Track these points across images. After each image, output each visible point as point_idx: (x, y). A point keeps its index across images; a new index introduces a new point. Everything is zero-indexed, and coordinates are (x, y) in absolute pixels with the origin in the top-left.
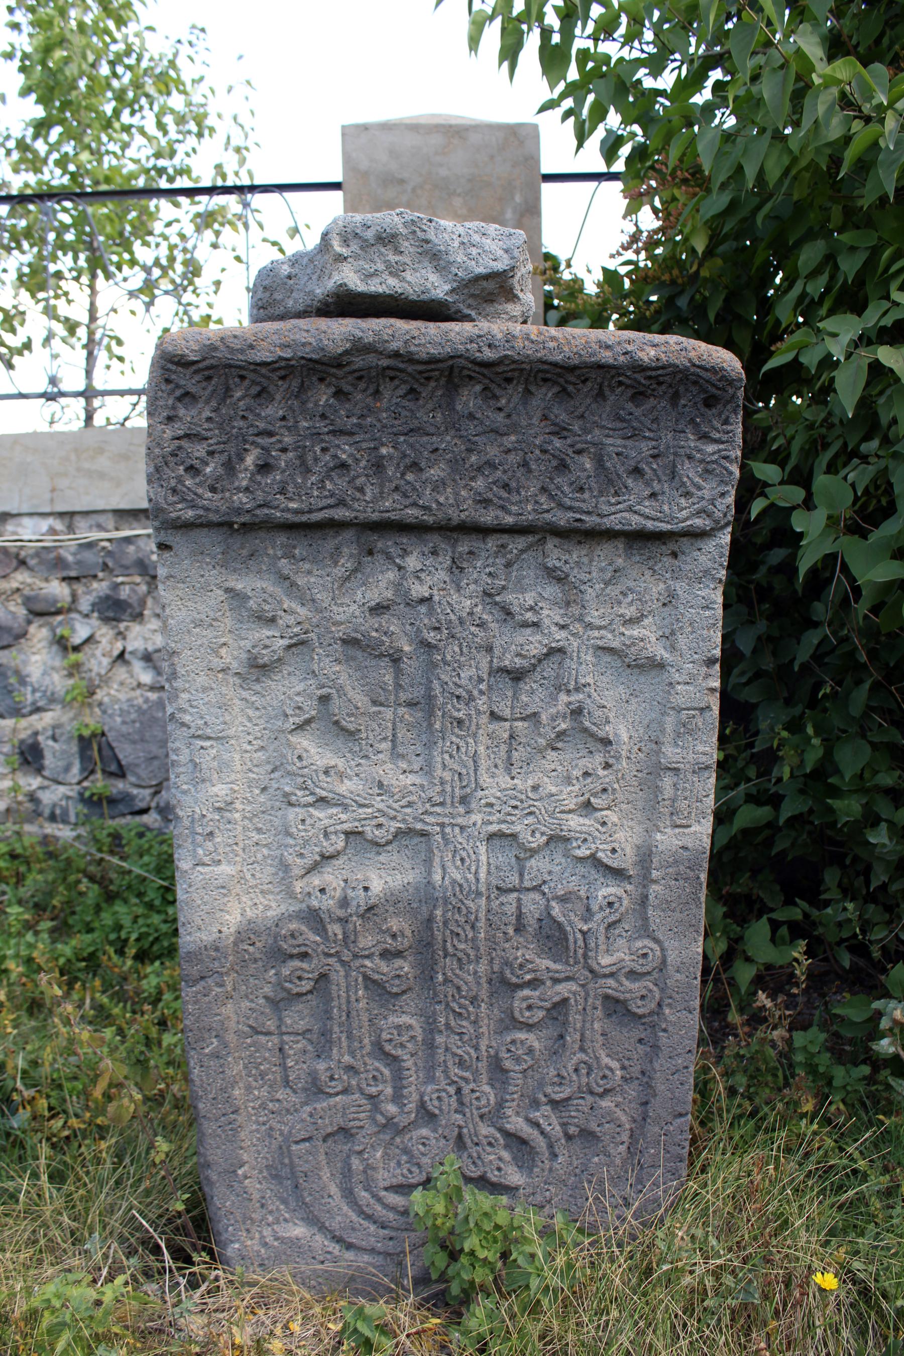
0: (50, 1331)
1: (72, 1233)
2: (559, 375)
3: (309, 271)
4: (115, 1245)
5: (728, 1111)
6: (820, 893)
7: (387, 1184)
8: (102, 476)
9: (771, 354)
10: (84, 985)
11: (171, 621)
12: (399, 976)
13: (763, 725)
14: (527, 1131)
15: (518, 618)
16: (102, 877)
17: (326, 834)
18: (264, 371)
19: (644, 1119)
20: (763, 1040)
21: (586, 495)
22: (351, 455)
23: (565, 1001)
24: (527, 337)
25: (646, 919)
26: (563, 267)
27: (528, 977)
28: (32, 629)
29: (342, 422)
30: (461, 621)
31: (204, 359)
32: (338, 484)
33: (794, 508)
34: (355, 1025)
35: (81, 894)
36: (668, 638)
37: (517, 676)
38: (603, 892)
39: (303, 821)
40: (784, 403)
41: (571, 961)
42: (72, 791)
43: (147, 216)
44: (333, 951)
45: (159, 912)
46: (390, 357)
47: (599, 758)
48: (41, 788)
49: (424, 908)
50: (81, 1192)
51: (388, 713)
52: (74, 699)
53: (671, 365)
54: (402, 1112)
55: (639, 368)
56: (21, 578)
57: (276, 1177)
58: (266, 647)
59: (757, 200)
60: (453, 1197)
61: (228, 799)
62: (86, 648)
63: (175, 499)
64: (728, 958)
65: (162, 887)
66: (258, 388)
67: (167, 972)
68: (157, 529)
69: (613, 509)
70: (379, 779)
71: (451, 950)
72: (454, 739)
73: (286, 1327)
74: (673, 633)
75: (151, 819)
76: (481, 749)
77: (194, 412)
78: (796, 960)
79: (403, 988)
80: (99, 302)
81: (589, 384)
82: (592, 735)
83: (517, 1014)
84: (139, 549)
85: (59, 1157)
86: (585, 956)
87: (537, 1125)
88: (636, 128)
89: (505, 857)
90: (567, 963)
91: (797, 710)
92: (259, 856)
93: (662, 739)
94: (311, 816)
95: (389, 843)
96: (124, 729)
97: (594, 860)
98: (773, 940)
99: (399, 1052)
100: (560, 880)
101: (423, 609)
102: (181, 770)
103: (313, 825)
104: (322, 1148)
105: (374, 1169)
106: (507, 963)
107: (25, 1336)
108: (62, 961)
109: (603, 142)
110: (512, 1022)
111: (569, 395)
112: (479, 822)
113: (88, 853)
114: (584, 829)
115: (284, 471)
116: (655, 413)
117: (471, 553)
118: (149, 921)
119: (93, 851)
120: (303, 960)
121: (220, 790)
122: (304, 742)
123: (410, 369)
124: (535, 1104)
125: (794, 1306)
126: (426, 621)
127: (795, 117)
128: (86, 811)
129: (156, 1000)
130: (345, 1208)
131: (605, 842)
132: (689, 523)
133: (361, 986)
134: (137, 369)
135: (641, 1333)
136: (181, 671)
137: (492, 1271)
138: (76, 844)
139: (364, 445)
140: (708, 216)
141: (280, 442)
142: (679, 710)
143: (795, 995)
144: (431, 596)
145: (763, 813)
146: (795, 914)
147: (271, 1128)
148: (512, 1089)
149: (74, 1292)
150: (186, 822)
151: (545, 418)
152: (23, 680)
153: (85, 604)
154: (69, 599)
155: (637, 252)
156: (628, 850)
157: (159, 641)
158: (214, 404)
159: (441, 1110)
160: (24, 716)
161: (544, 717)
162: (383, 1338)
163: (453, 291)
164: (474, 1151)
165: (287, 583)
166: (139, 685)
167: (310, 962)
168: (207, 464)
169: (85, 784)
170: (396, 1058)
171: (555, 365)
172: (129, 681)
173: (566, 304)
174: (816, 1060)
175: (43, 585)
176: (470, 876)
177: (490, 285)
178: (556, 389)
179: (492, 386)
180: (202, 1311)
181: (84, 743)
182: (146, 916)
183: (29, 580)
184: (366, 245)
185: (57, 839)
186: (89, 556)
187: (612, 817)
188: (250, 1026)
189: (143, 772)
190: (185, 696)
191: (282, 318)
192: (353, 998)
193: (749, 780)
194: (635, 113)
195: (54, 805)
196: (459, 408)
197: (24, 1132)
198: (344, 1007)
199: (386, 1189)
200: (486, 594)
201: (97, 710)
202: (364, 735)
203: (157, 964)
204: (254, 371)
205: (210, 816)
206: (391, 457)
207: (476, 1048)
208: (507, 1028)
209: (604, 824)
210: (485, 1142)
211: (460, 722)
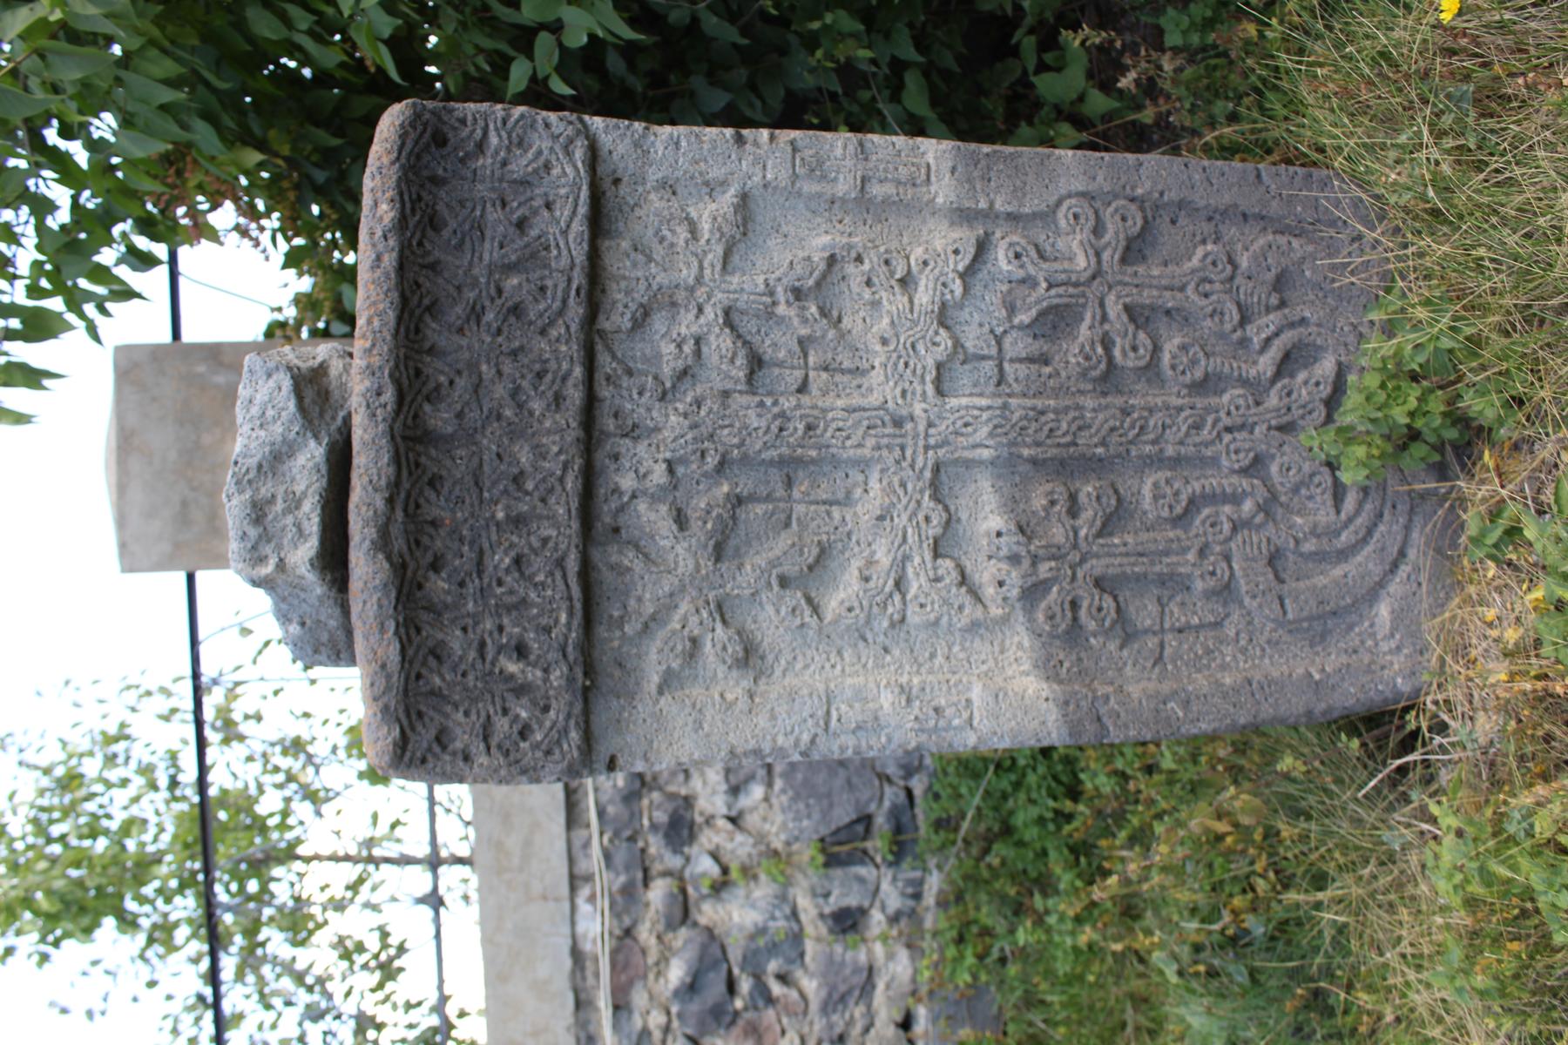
0: (1489, 885)
1: (1383, 864)
2: (412, 314)
3: (296, 602)
4: (1396, 816)
5: (1255, 122)
6: (1005, 16)
7: (1332, 511)
8: (528, 843)
9: (381, 70)
10: (1106, 859)
11: (696, 756)
12: (1098, 498)
13: (810, 81)
14: (1274, 352)
15: (690, 361)
16: (985, 839)
17: (937, 580)
18: (410, 652)
19: (1263, 218)
20: (1174, 82)
21: (549, 283)
22: (506, 553)
23: (1127, 308)
24: (368, 351)
25: (1035, 216)
26: (280, 317)
27: (1100, 350)
28: (703, 921)
29: (467, 560)
30: (694, 426)
31: (398, 720)
32: (539, 568)
33: (560, 45)
34: (1153, 547)
35: (1003, 863)
36: (712, 188)
37: (756, 363)
38: (1004, 265)
39: (922, 606)
40: (434, 56)
41: (1081, 301)
42: (887, 875)
43: (225, 797)
44: (1069, 572)
45: (1024, 775)
46: (393, 509)
47: (851, 269)
48: (883, 909)
49: (1021, 469)
50: (1337, 855)
51: (799, 509)
52: (782, 873)
53: (398, 185)
54: (1252, 494)
55: (402, 223)
56: (645, 934)
57: (1323, 636)
58: (724, 648)
59: (201, 89)
60: (1348, 436)
61: (897, 690)
62: (725, 859)
63: (557, 751)
64: (1080, 122)
65: (996, 772)
66: (431, 658)
67: (1093, 765)
68: (592, 772)
69: (564, 252)
70: (875, 522)
71: (1068, 439)
72: (829, 434)
73: (1490, 625)
74: (707, 184)
75: (918, 785)
76: (840, 403)
77: (458, 731)
78: (1083, 43)
79: (1111, 492)
80: (326, 852)
81: (421, 280)
82: (824, 276)
83: (1142, 363)
84: (611, 801)
85: (1298, 880)
86: (1076, 285)
87: (1268, 341)
88: (117, 230)
89: (963, 377)
90: (1084, 306)
91: (792, 38)
92: (962, 655)
93: (828, 196)
94: (916, 597)
95: (946, 509)
96: (816, 816)
97: (966, 275)
98: (1059, 70)
99: (1184, 497)
100: (989, 313)
101: (680, 470)
102: (864, 744)
103: (927, 595)
104: (1292, 584)
105: (1315, 526)
106: (1084, 374)
107: (1493, 912)
108: (1079, 883)
109: (135, 269)
110: (1151, 370)
111: (434, 303)
112: (924, 405)
113: (957, 856)
114: (931, 285)
115: (525, 629)
116: (454, 203)
117: (616, 416)
118: (1034, 786)
119: (954, 850)
120: (1078, 608)
121: (887, 700)
122: (832, 604)
123: (406, 485)
124: (1244, 342)
125: (1478, 45)
126: (694, 466)
127: (101, 42)
128: (909, 859)
129: (1124, 777)
130: (1359, 558)
131: (946, 261)
132: (580, 165)
133: (1108, 541)
134: (406, 796)
135: (1504, 221)
136: (752, 744)
137: (1431, 391)
138: (947, 868)
139: (494, 537)
140: (219, 144)
141: (491, 633)
142: (795, 176)
143: (1123, 45)
144: (666, 460)
145: (913, 81)
146: (1028, 44)
147: (1269, 642)
148: (1226, 369)
149: (1447, 858)
150: (923, 738)
151: (460, 331)
152: (761, 931)
153: (675, 862)
154: (668, 880)
155: (262, 229)
156: (956, 235)
157: (715, 776)
158: (449, 709)
159: (1250, 450)
160: (801, 929)
161: (804, 331)
162: (1506, 514)
163: (316, 437)
164: (1297, 413)
165: (652, 625)
166: (766, 799)
167: (1081, 598)
168: (517, 716)
169: (878, 859)
170: (1191, 501)
171: (399, 319)
172: (761, 811)
173: (329, 309)
174: (1198, 20)
175: (652, 908)
176: (985, 416)
177: (309, 394)
178: (427, 318)
179: (425, 391)
180: (1471, 718)
181: (832, 861)
182: (1029, 791)
183: (648, 925)
184: (266, 537)
185: (941, 892)
186: (620, 857)
187: (917, 254)
188: (1154, 665)
189: (865, 795)
190: (780, 740)
191: (349, 633)
192: (1122, 549)
193: (874, 99)
194: (100, 231)
195: (903, 894)
196: (450, 430)
197: (1269, 920)
198: (1132, 559)
199: (1338, 512)
200: (663, 398)
201: (795, 847)
202: (825, 537)
203: (1082, 776)
204: (411, 663)
205: (916, 711)
206: (507, 508)
207: (1180, 409)
208: (1158, 375)
209: (925, 263)
210: (1286, 400)
211: (809, 428)
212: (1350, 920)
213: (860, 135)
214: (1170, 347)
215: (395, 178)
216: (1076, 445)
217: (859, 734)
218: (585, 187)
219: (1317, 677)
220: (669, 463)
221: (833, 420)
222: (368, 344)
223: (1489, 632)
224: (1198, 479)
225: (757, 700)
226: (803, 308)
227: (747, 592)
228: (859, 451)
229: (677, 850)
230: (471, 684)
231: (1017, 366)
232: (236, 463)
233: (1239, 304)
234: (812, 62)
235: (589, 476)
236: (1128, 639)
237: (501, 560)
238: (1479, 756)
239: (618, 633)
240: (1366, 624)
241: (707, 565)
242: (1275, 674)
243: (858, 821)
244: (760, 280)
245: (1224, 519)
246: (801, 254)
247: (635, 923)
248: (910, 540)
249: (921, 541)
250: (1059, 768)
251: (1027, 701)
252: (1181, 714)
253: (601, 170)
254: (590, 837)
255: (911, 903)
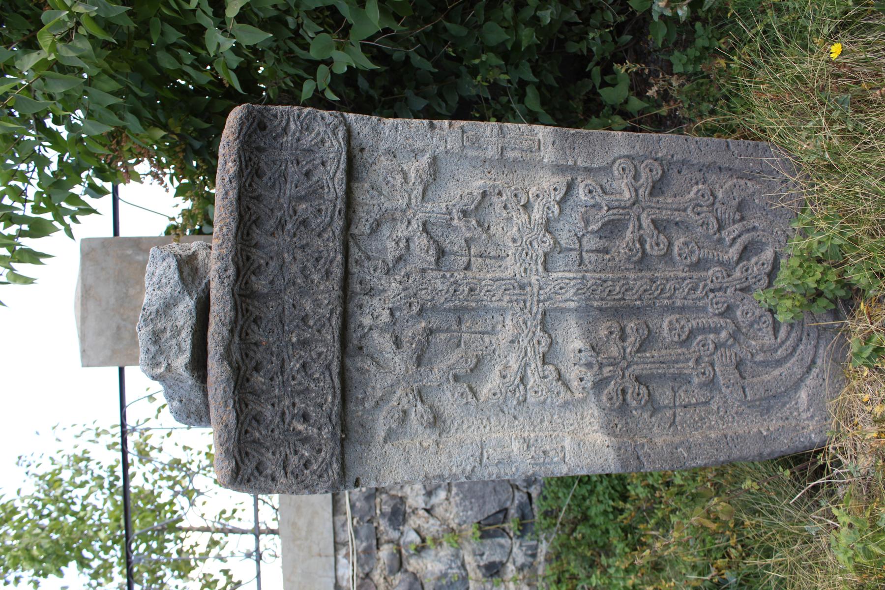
0: (869, 558)
1: (805, 543)
2: (245, 225)
3: (177, 389)
5: (725, 115)
7: (773, 337)
8: (310, 524)
9: (231, 87)
11: (405, 479)
15: (403, 252)
17: (545, 377)
18: (242, 418)
19: (730, 170)
20: (678, 91)
21: (323, 207)
22: (297, 361)
23: (653, 221)
27: (638, 245)
28: (411, 569)
29: (275, 361)
31: (235, 457)
32: (316, 370)
33: (332, 72)
34: (669, 358)
35: (583, 537)
36: (416, 154)
37: (441, 253)
38: (582, 197)
39: (536, 392)
40: (263, 78)
41: (627, 217)
42: (517, 543)
44: (621, 373)
45: (595, 487)
47: (495, 199)
48: (514, 563)
50: (778, 537)
51: (466, 336)
52: (456, 542)
53: (238, 152)
54: (726, 327)
57: (768, 410)
58: (422, 416)
59: (131, 96)
60: (781, 294)
61: (521, 441)
62: (423, 534)
63: (325, 476)
64: (625, 115)
65: (579, 484)
66: (253, 422)
67: (635, 481)
68: (345, 488)
69: (332, 190)
70: (508, 343)
71: (620, 296)
72: (482, 294)
73: (866, 403)
74: (413, 151)
75: (534, 491)
76: (489, 276)
78: (626, 70)
79: (645, 327)
81: (250, 206)
82: (480, 203)
83: (662, 253)
86: (624, 208)
87: (734, 239)
88: (84, 175)
89: (560, 261)
90: (629, 220)
91: (463, 69)
92: (559, 421)
94: (533, 387)
96: (476, 509)
97: (561, 203)
98: (613, 86)
99: (687, 329)
100: (575, 224)
101: (397, 314)
102: (502, 472)
105: (763, 346)
106: (629, 259)
107: (872, 574)
108: (627, 550)
109: (93, 197)
110: (667, 256)
111: (258, 219)
112: (537, 277)
113: (557, 533)
115: (308, 405)
117: (361, 283)
118: (601, 493)
119: (555, 529)
120: (626, 393)
121: (516, 446)
122: (484, 391)
124: (720, 241)
126: (405, 312)
127: (77, 71)
128: (529, 534)
129: (653, 488)
130: (788, 365)
131: (550, 195)
132: (341, 140)
135: (870, 172)
136: (438, 472)
137: (829, 269)
139: (291, 352)
140: (141, 128)
141: (288, 407)
143: (650, 71)
144: (389, 308)
146: (596, 71)
147: (736, 413)
148: (711, 256)
149: (843, 541)
150: (537, 468)
151: (273, 234)
152: (444, 575)
153: (395, 535)
154: (391, 545)
156: (555, 180)
157: (418, 486)
158: (263, 450)
159: (724, 302)
160: (467, 574)
161: (468, 235)
162: (873, 340)
163: (190, 294)
166: (447, 499)
168: (303, 455)
169: (512, 534)
170: (691, 332)
171: (238, 228)
172: (444, 506)
173: (198, 221)
175: (382, 562)
176: (572, 283)
177: (186, 270)
178: (254, 227)
179: (252, 269)
180: (856, 458)
181: (485, 535)
182: (598, 495)
183: (379, 571)
184: (160, 351)
185: (547, 553)
186: (363, 532)
187: (533, 190)
190: (454, 470)
191: (207, 406)
192: (651, 360)
193: (509, 101)
194: (74, 176)
195: (526, 555)
196: (266, 291)
198: (657, 365)
202: (480, 353)
203: (629, 487)
204: (242, 424)
205: (533, 453)
206: (299, 335)
207: (684, 279)
208: (671, 259)
209: (538, 196)
210: (745, 274)
211: (471, 290)
212: (788, 577)
213: (500, 124)
214: (678, 244)
215: (236, 148)
216: (625, 300)
217: (499, 466)
218: (344, 153)
219: (765, 433)
220: (391, 309)
221: (485, 285)
222: (220, 242)
223: (865, 408)
224: (694, 319)
225: (441, 446)
226: (468, 222)
227: (436, 384)
228: (500, 303)
229: (396, 528)
230: (277, 436)
231: (591, 254)
232: (144, 309)
233: (717, 219)
234: (475, 82)
235: (345, 318)
236: (655, 411)
237: (295, 365)
238: (861, 480)
239: (361, 408)
240: (793, 403)
241: (412, 369)
242: (741, 432)
243: (500, 512)
244: (444, 205)
245: (710, 342)
246: (467, 191)
247: (371, 570)
248: (529, 355)
249: (535, 355)
250: (616, 482)
251: (597, 447)
252: (686, 455)
253: (353, 143)
254: (347, 520)
255: (530, 559)
